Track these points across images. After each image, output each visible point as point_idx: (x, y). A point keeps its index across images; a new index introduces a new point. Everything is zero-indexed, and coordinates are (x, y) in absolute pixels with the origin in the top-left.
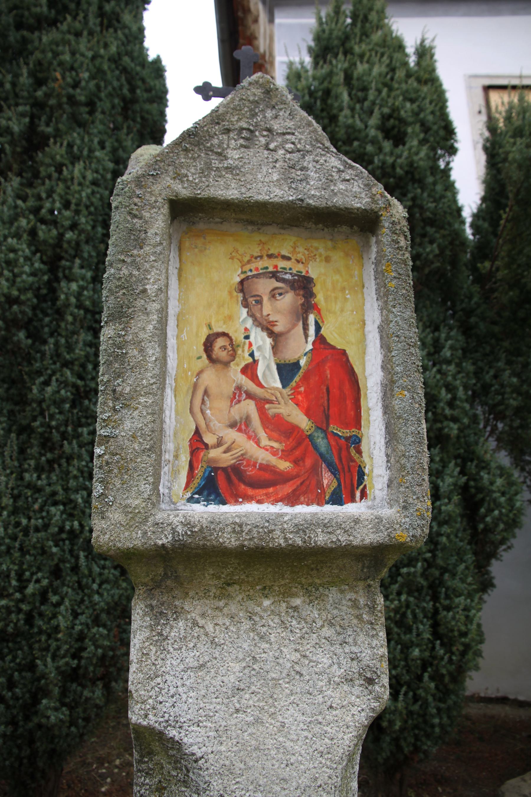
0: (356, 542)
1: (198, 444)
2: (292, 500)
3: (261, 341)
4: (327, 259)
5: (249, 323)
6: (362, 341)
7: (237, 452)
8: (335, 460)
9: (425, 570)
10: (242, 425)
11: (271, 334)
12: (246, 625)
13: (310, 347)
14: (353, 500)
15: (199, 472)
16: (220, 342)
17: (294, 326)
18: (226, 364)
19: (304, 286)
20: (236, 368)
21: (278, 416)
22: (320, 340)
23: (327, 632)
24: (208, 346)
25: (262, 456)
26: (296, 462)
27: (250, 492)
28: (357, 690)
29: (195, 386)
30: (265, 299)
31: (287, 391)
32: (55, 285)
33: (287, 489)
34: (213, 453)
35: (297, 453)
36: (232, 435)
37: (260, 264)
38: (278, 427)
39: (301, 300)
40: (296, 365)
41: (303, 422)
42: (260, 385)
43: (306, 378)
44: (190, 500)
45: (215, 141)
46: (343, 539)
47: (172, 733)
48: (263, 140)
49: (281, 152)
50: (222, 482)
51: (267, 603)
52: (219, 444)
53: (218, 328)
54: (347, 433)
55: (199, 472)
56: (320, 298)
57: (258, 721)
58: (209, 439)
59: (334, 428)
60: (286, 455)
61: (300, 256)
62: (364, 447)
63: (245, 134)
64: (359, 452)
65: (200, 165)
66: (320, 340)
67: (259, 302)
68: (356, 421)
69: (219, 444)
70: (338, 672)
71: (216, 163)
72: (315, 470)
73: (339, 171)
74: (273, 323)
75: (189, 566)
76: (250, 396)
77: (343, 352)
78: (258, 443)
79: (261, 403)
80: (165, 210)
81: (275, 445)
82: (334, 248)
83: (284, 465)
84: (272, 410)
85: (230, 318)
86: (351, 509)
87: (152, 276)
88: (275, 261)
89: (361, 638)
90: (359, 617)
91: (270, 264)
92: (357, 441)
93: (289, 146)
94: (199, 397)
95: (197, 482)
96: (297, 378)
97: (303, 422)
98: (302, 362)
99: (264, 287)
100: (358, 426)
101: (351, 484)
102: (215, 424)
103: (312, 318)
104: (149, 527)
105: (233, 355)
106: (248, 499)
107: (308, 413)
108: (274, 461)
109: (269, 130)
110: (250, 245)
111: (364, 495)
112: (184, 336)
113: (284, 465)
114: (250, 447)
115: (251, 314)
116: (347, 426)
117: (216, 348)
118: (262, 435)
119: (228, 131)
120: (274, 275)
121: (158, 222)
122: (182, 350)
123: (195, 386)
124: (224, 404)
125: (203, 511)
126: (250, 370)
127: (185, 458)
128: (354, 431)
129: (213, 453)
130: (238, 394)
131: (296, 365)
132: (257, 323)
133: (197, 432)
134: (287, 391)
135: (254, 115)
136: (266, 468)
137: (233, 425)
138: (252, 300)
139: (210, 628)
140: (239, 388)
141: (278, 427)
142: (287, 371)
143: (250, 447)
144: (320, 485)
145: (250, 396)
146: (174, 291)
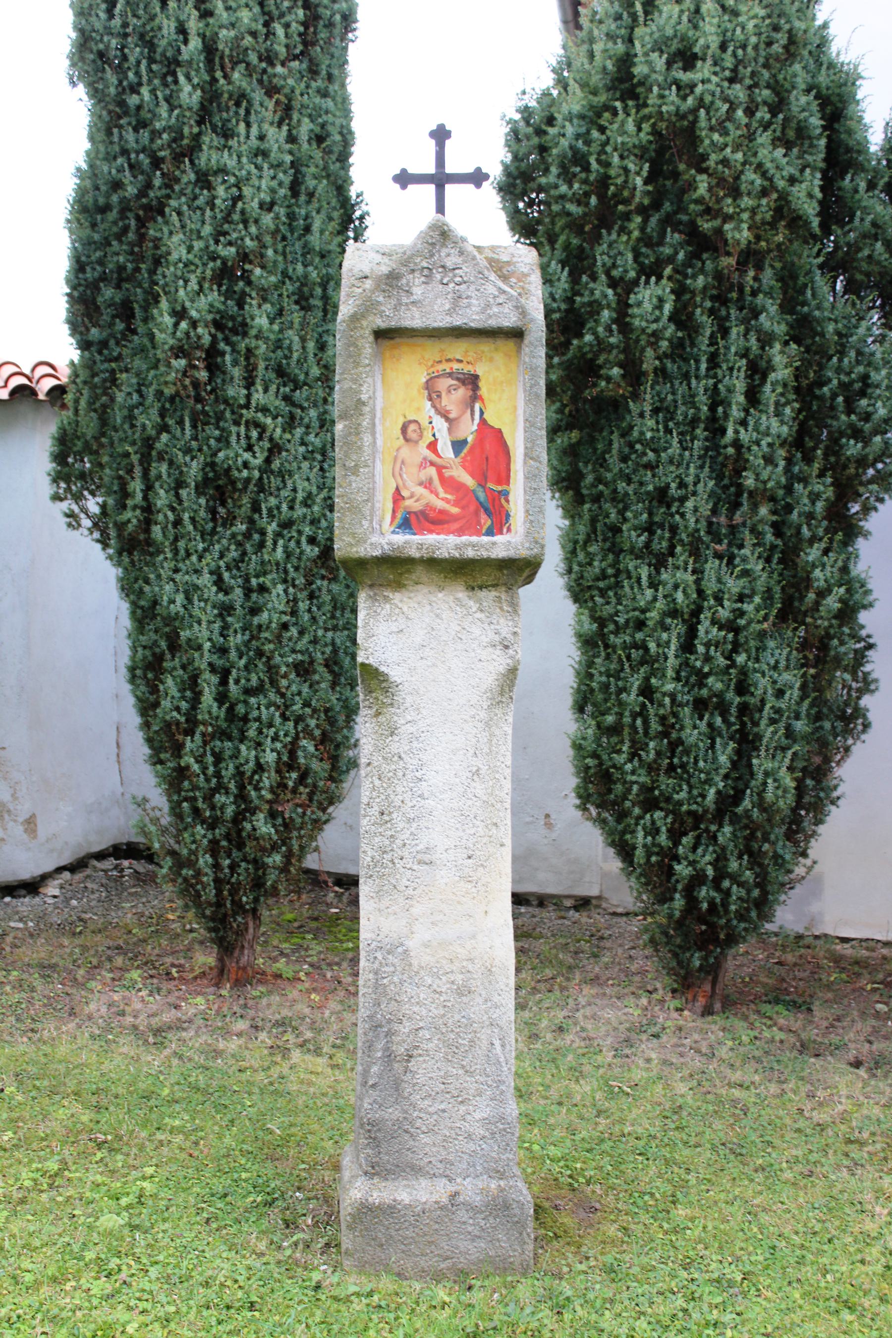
0: (493, 556)
1: (398, 497)
2: (460, 532)
3: (440, 424)
4: (491, 360)
5: (432, 412)
6: (514, 422)
7: (423, 502)
8: (489, 506)
9: (646, 649)
10: (428, 485)
11: (447, 419)
12: (428, 608)
13: (475, 427)
14: (501, 532)
15: (399, 516)
16: (412, 427)
17: (464, 412)
18: (416, 442)
19: (472, 381)
20: (423, 444)
21: (452, 478)
22: (483, 422)
23: (479, 615)
24: (404, 429)
25: (440, 504)
26: (463, 508)
27: (432, 527)
28: (498, 652)
29: (396, 458)
30: (444, 394)
31: (458, 460)
32: (353, 438)
33: (456, 526)
34: (408, 503)
35: (464, 502)
36: (421, 490)
37: (440, 367)
38: (449, 483)
39: (470, 393)
40: (465, 442)
41: (469, 481)
42: (439, 456)
43: (472, 448)
44: (393, 532)
45: (404, 281)
46: (485, 554)
47: (382, 669)
48: (438, 276)
49: (452, 285)
50: (413, 520)
51: (440, 595)
52: (412, 497)
53: (411, 417)
54: (500, 488)
55: (399, 516)
56: (484, 391)
57: (434, 665)
58: (405, 493)
59: (490, 485)
60: (456, 504)
61: (470, 359)
62: (511, 498)
63: (426, 272)
64: (508, 501)
65: (393, 302)
66: (483, 422)
67: (439, 396)
68: (505, 478)
69: (412, 497)
70: (485, 640)
71: (405, 300)
72: (476, 513)
73: (495, 297)
74: (448, 412)
75: (394, 570)
76: (432, 464)
77: (500, 431)
78: (437, 495)
79: (440, 469)
80: (371, 338)
81: (449, 496)
82: (496, 349)
83: (455, 510)
84: (447, 473)
85: (419, 409)
86: (498, 538)
87: (364, 389)
88: (450, 365)
89: (502, 621)
90: (501, 608)
91: (446, 367)
92: (506, 494)
93: (458, 279)
94: (399, 465)
95: (399, 520)
96: (465, 451)
97: (469, 481)
98: (470, 439)
99: (445, 383)
100: (508, 483)
101: (499, 520)
102: (409, 483)
103: (477, 406)
104: (367, 546)
105: (421, 436)
106: (431, 532)
107: (473, 477)
108: (447, 507)
109: (443, 267)
110: (432, 350)
111: (509, 530)
112: (388, 424)
113: (455, 510)
114: (432, 499)
115: (434, 406)
116: (499, 483)
117: (408, 431)
118: (440, 490)
119: (413, 271)
120: (450, 375)
121: (367, 346)
122: (385, 435)
123: (396, 458)
124: (415, 470)
125: (400, 538)
126: (433, 446)
127: (390, 505)
128: (505, 487)
129: (408, 503)
130: (426, 462)
131: (465, 442)
132: (439, 412)
133: (397, 489)
134: (458, 460)
135: (432, 256)
136: (442, 512)
137: (421, 484)
138: (434, 396)
139: (405, 609)
140: (425, 459)
141: (449, 483)
142: (458, 445)
143: (432, 499)
144: (479, 523)
145: (432, 464)
146: (379, 394)
